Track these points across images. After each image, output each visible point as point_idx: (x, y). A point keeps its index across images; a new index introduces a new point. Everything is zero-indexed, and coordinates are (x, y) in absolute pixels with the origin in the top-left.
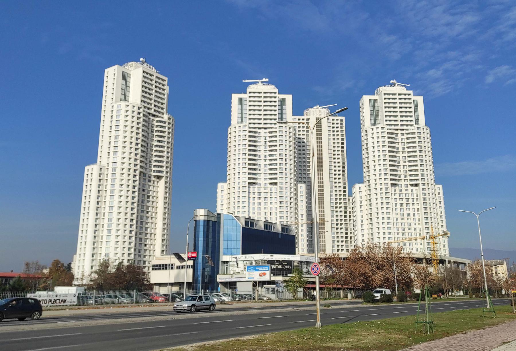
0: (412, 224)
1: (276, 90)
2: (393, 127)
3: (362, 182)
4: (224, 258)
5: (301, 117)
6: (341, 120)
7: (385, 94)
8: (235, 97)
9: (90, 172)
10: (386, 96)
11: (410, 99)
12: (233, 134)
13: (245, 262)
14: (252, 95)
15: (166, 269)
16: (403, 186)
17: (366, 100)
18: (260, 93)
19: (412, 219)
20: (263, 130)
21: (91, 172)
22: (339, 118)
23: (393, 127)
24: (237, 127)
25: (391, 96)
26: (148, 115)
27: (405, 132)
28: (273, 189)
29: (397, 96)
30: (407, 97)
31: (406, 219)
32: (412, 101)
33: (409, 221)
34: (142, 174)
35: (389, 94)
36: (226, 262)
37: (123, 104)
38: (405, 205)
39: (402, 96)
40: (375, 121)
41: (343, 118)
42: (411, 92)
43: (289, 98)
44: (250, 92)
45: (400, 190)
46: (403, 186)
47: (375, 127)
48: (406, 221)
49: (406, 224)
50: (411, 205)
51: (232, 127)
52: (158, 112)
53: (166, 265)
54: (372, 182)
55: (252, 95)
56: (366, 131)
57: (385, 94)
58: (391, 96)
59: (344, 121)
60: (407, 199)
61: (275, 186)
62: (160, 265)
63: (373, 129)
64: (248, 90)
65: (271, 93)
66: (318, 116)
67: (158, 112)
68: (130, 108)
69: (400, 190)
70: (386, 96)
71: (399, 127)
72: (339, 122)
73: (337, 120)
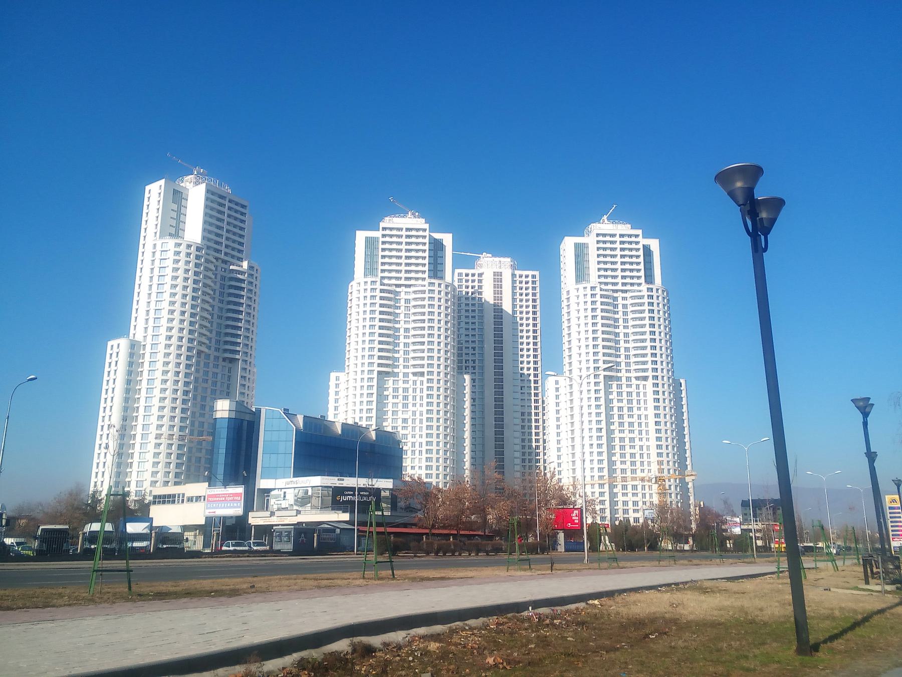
0: (637, 440)
1: (427, 226)
2: (610, 287)
3: (559, 372)
4: (263, 483)
5: (470, 271)
6: (534, 276)
7: (598, 235)
8: (361, 236)
9: (115, 350)
10: (601, 238)
11: (637, 243)
12: (355, 294)
13: (297, 490)
14: (388, 232)
15: (173, 502)
16: (624, 379)
17: (568, 245)
18: (400, 229)
19: (636, 432)
20: (403, 288)
21: (117, 350)
22: (530, 273)
23: (610, 287)
24: (362, 284)
25: (608, 238)
26: (214, 261)
27: (628, 295)
28: (418, 383)
29: (618, 239)
30: (633, 239)
31: (627, 432)
32: (640, 246)
33: (632, 435)
34: (203, 355)
35: (604, 235)
36: (268, 491)
37: (171, 243)
38: (625, 410)
39: (626, 239)
40: (581, 274)
41: (537, 273)
42: (639, 232)
43: (447, 239)
44: (384, 229)
45: (619, 386)
46: (624, 379)
47: (581, 286)
48: (627, 435)
49: (627, 440)
50: (635, 409)
51: (353, 283)
52: (233, 257)
53: (174, 496)
54: (576, 373)
55: (388, 232)
56: (568, 292)
57: (598, 235)
58: (608, 238)
59: (538, 278)
60: (630, 401)
61: (421, 378)
62: (164, 496)
63: (578, 290)
64: (382, 225)
65: (418, 230)
66: (496, 270)
67: (233, 257)
68: (183, 248)
69: (619, 386)
70: (601, 238)
71: (619, 287)
72: (530, 279)
73: (527, 276)
